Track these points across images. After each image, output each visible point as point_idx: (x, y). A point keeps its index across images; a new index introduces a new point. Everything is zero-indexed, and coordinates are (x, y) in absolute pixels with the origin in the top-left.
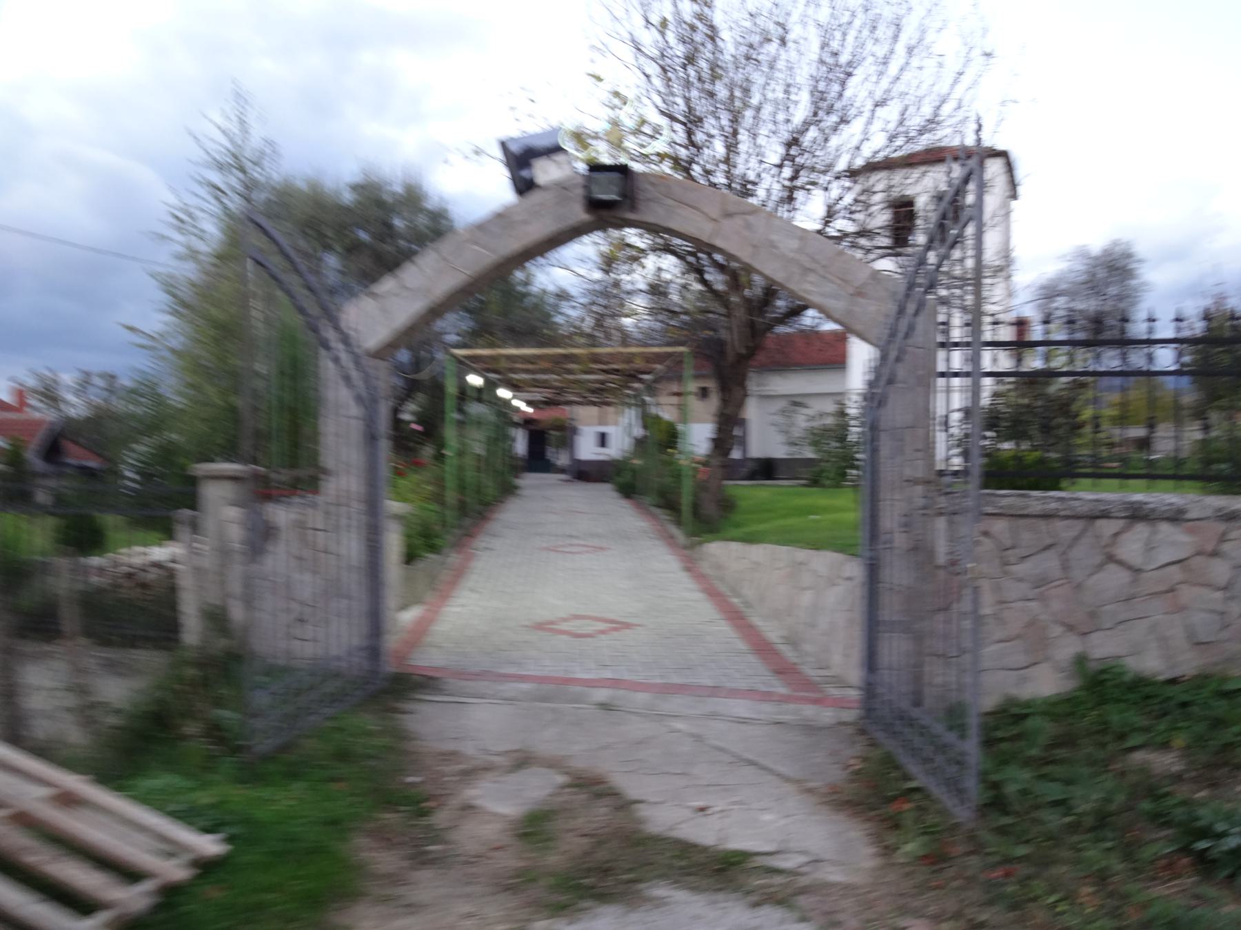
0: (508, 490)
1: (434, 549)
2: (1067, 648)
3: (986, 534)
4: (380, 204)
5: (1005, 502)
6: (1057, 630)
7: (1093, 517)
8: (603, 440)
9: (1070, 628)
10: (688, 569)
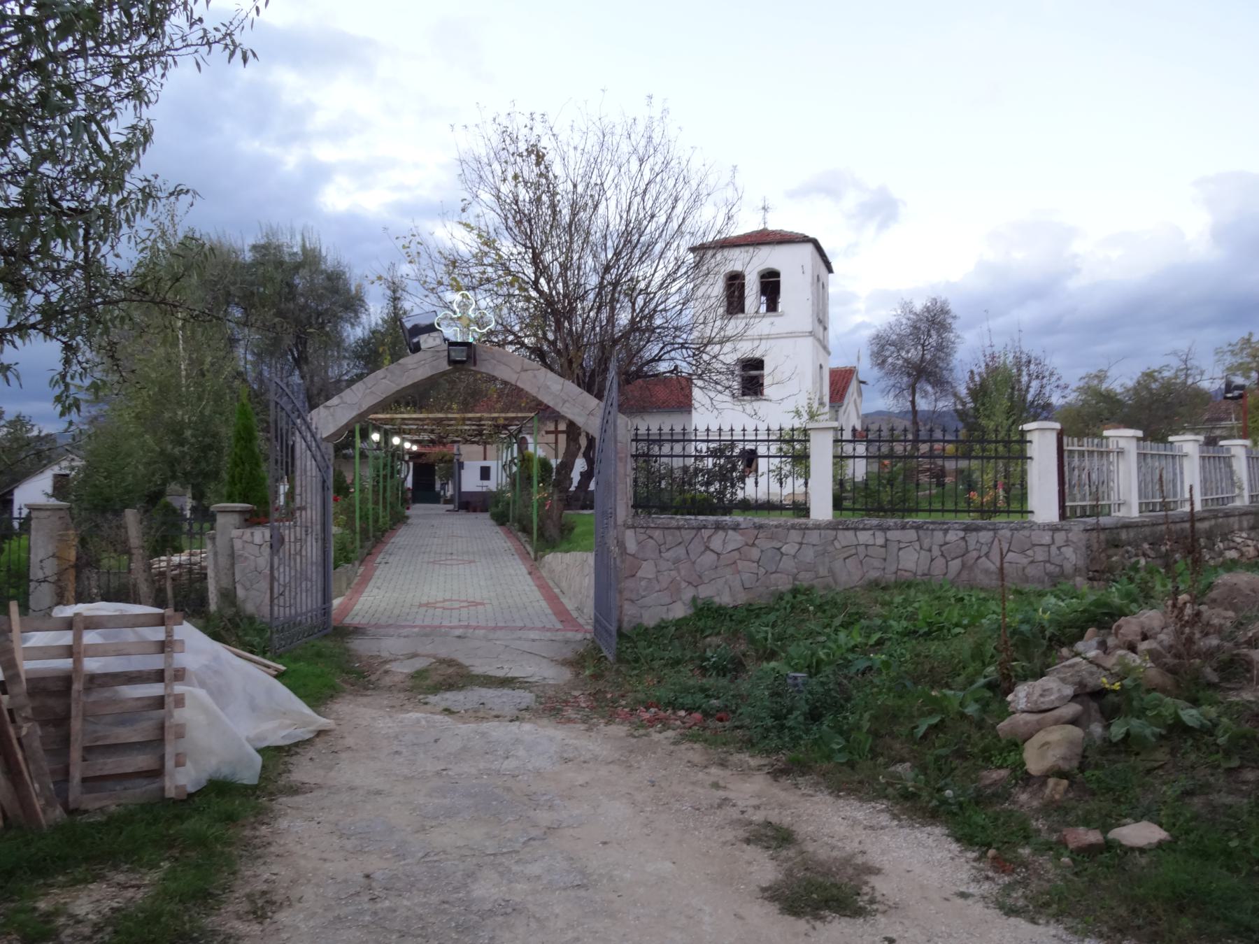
0: (399, 519)
1: (348, 560)
2: (688, 594)
3: (651, 537)
4: (280, 264)
5: (659, 521)
6: (684, 585)
7: (699, 529)
8: (485, 473)
9: (690, 583)
10: (530, 573)
